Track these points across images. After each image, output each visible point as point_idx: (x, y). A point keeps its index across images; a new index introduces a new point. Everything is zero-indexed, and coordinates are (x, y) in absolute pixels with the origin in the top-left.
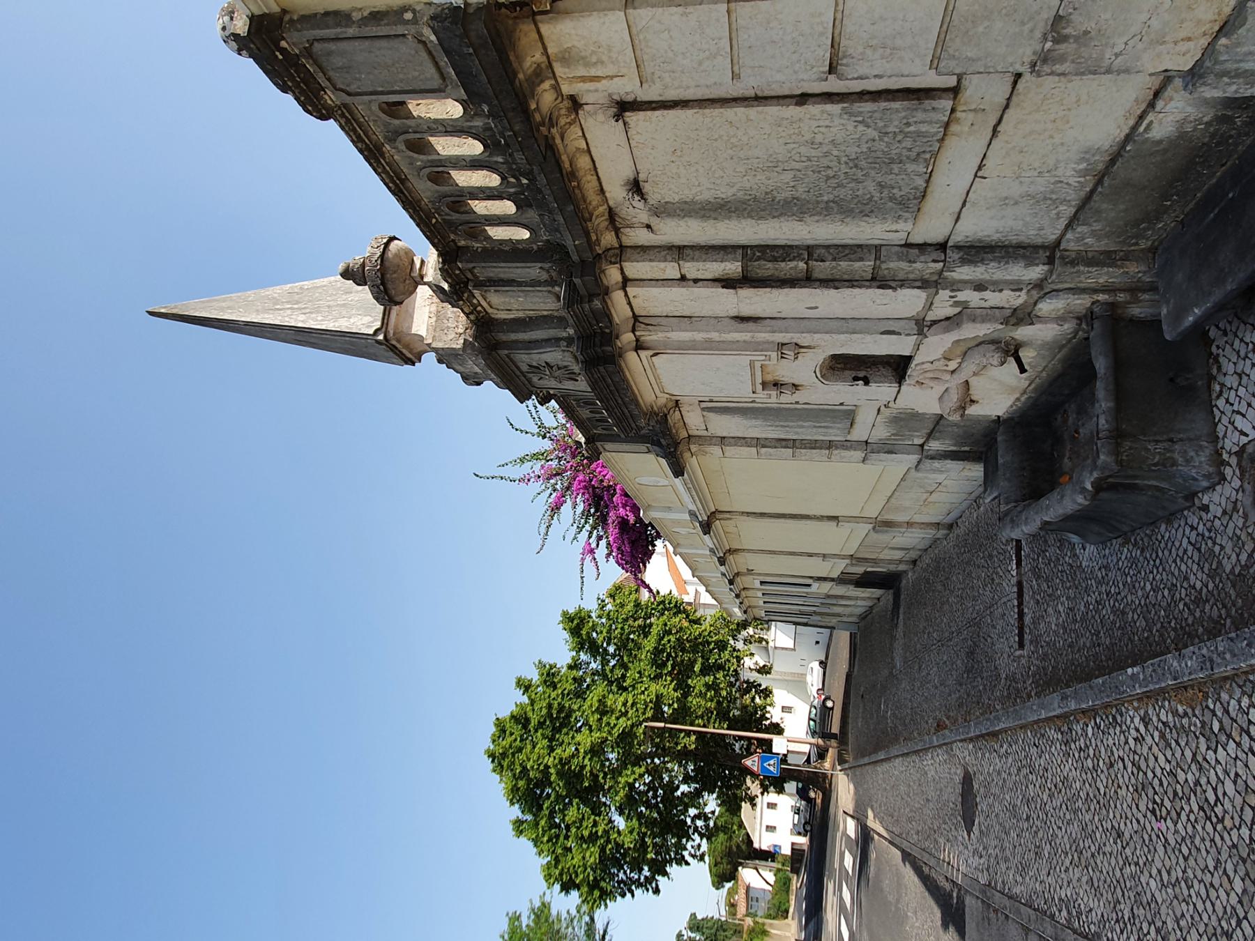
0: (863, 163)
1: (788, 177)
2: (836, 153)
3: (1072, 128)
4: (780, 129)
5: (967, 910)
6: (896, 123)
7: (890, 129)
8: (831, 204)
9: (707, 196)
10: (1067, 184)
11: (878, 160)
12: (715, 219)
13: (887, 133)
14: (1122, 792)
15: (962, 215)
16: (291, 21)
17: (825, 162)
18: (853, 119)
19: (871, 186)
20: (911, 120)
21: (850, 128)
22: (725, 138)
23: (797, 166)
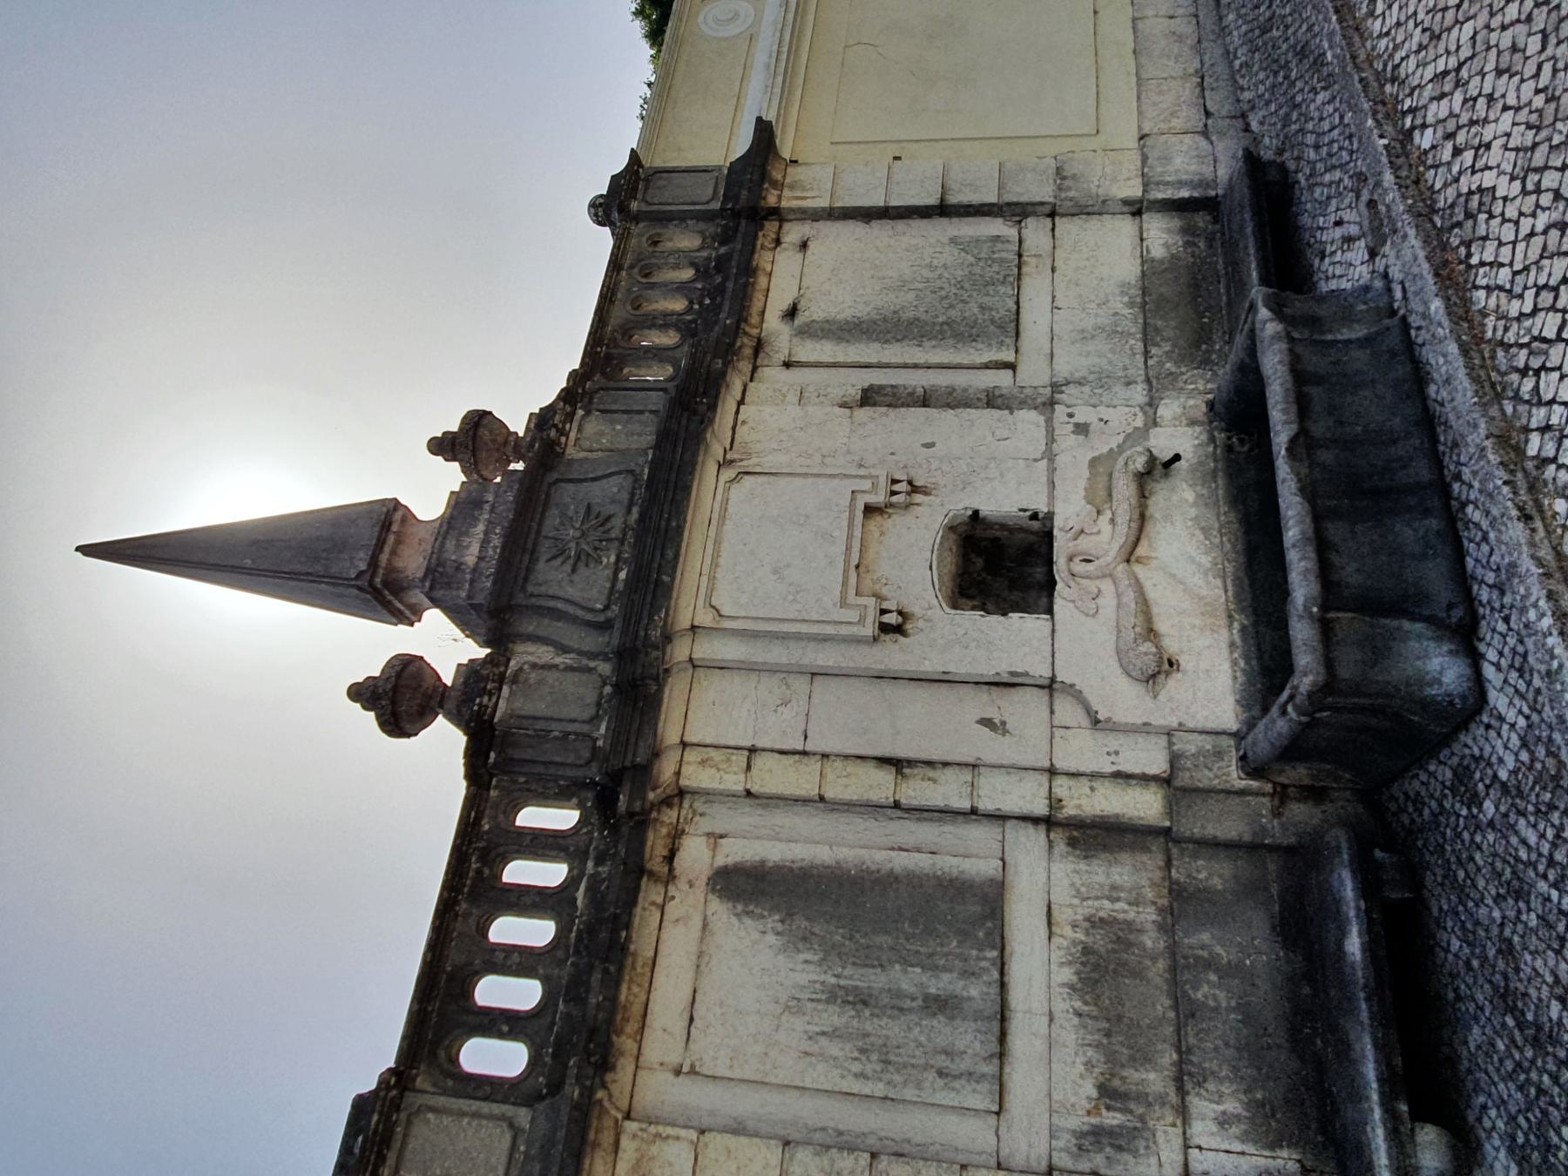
1: (912, 295)
2: (946, 275)
9: (847, 314)
17: (939, 283)
23: (920, 286)
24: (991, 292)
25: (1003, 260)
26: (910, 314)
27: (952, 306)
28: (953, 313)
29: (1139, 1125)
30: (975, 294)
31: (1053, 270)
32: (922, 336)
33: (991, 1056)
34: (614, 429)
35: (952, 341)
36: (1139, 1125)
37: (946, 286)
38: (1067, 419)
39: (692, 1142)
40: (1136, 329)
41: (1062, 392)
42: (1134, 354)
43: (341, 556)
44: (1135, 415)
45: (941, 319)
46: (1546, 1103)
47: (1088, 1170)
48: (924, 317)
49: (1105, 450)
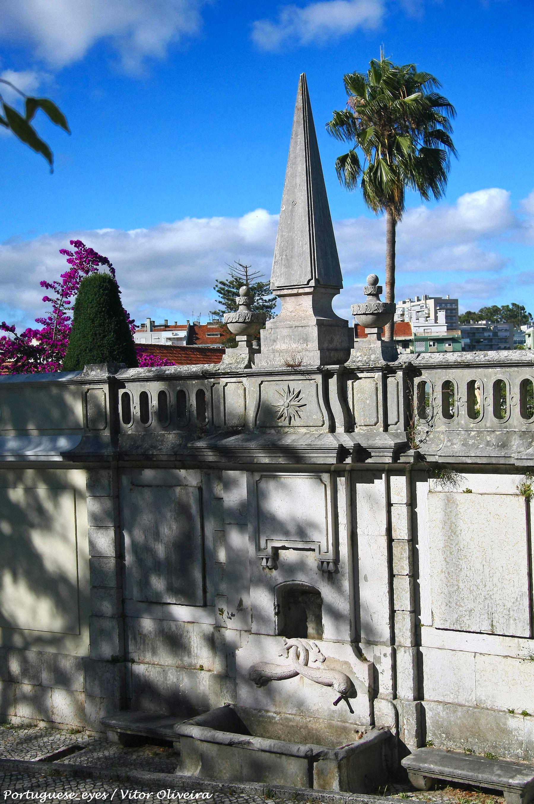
0: (487, 601)
1: (478, 566)
2: (495, 589)
3: (510, 687)
4: (513, 565)
5: (118, 634)
6: (516, 615)
7: (511, 613)
8: (456, 587)
9: (462, 525)
10: (471, 694)
11: (490, 609)
12: (443, 528)
13: (509, 611)
14: (437, 555)
15: (444, 651)
16: (87, 693)
17: (489, 584)
18: (519, 597)
19: (471, 606)
20: (517, 621)
21: (513, 596)
22: (507, 540)
23: (487, 572)
24: (482, 617)
25: (508, 625)
26: (463, 564)
27: (471, 592)
28: (466, 593)
29: (349, 160)
30: (481, 606)
31: (506, 657)
32: (449, 573)
33: (147, 599)
34: (367, 399)
35: (446, 591)
36: (349, 160)
37: (487, 588)
38: (383, 653)
39: (110, 495)
40: (461, 700)
41: (405, 652)
42: (443, 696)
43: (283, 267)
44: (387, 689)
45: (461, 585)
46: (85, 263)
47: (302, 754)
48: (463, 574)
49: (354, 670)
